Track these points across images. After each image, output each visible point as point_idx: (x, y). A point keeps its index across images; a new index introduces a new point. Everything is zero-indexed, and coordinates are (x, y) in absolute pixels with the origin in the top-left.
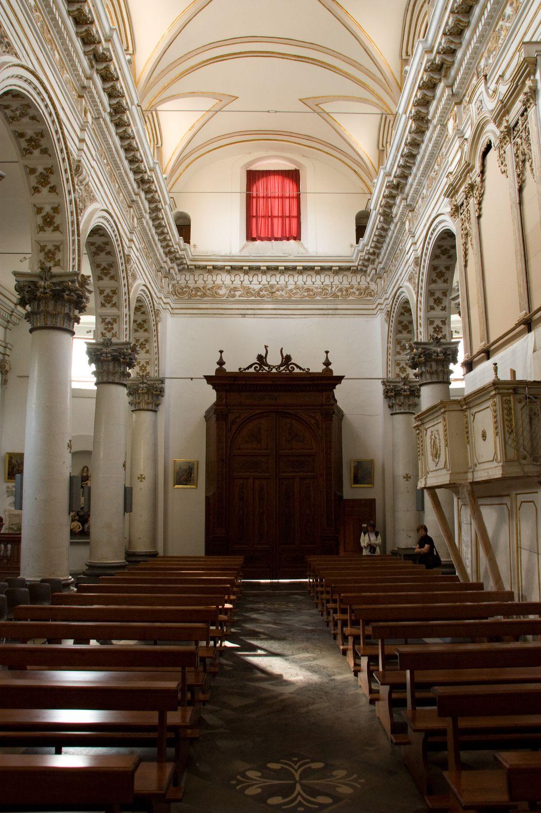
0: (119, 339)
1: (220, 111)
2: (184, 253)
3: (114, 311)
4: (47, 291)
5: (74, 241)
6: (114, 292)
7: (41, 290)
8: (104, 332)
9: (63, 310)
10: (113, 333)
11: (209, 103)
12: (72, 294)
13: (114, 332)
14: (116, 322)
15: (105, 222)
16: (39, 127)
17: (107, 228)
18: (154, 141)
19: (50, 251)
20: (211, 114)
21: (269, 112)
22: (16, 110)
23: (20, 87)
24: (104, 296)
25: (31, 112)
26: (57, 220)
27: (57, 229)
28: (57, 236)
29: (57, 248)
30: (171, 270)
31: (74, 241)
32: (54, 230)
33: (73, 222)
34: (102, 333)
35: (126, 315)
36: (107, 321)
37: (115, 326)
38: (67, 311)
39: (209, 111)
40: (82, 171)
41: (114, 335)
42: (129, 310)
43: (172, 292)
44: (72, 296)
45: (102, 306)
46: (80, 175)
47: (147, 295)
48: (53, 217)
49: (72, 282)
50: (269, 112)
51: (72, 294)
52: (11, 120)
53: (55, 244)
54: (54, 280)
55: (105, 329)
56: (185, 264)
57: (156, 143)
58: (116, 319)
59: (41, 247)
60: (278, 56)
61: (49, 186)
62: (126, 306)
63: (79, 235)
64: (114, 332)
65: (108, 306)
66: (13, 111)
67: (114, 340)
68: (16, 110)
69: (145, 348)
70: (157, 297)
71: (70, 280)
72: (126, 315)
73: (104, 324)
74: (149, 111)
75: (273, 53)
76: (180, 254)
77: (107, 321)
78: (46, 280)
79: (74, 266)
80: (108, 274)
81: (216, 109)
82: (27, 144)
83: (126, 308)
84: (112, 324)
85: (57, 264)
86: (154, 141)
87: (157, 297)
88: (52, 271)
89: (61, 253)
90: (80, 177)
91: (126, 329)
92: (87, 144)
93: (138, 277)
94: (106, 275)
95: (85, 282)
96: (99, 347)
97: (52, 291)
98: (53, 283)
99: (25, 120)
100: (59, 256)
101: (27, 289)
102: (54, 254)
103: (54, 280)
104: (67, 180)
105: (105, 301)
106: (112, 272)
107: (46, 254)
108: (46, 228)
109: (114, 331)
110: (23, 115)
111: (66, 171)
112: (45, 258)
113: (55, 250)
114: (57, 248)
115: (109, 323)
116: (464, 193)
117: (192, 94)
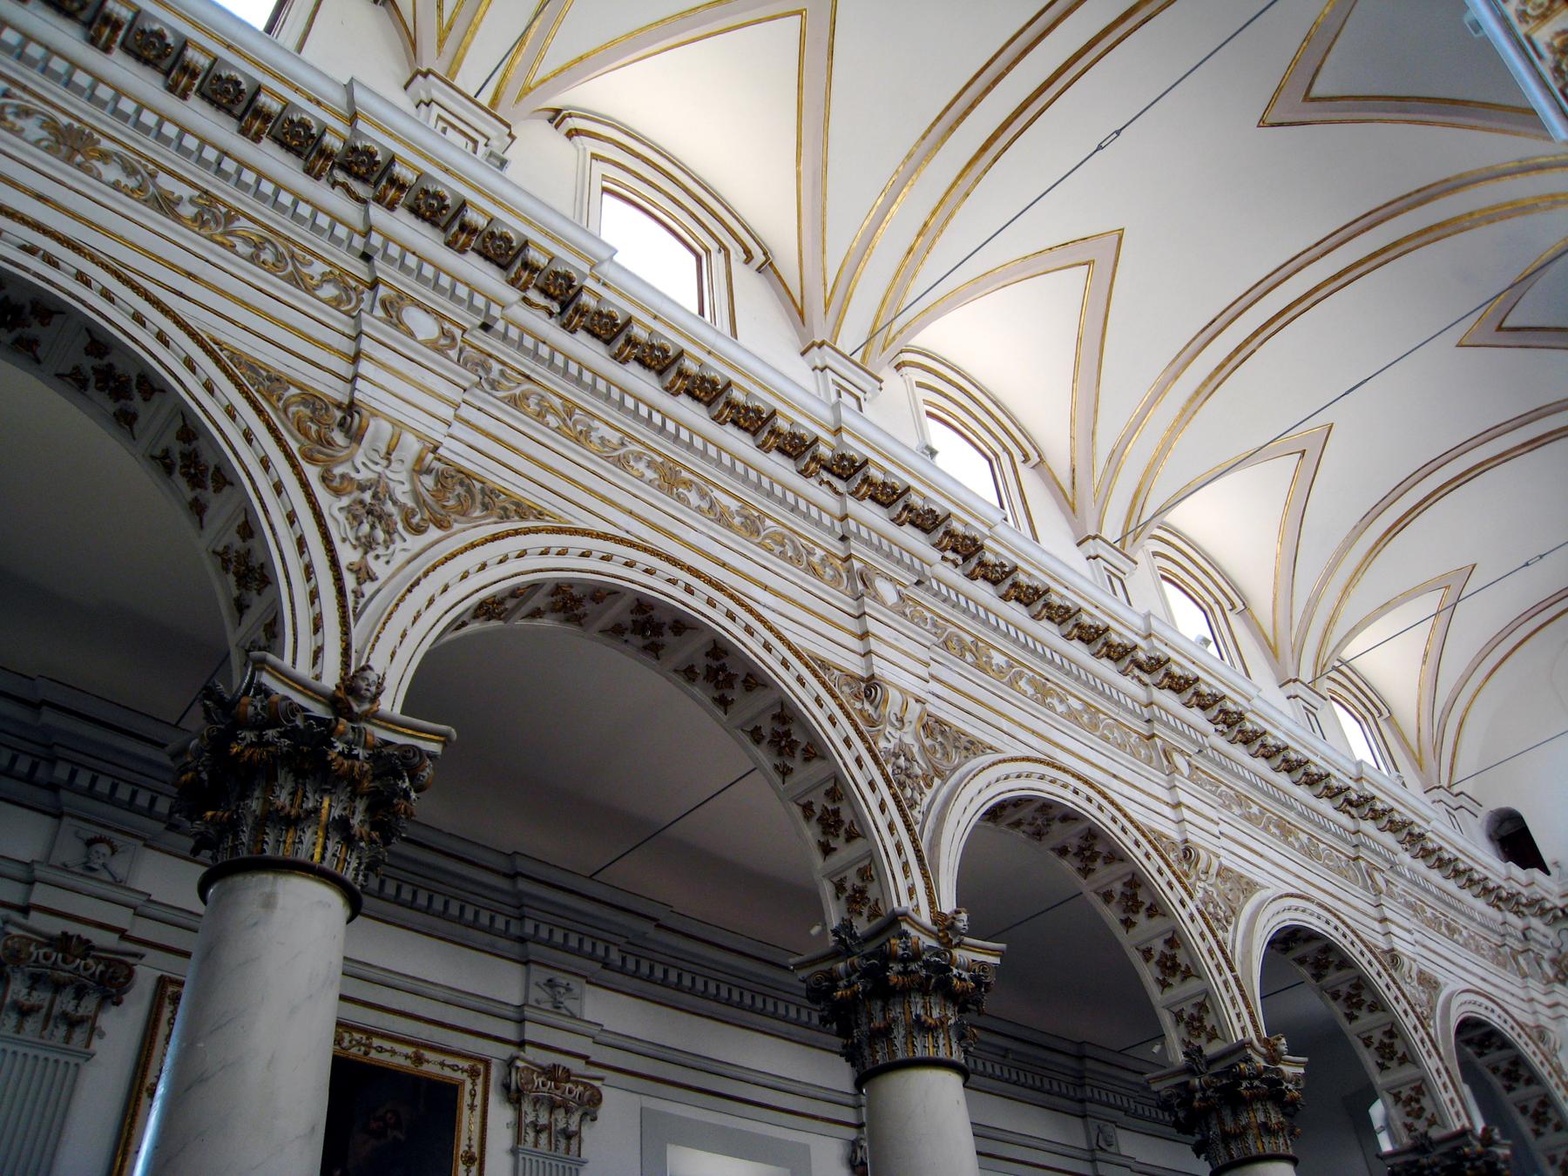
0: (1445, 1127)
1: (1458, 601)
2: (1531, 889)
3: (1408, 1072)
4: (1209, 1093)
5: (1226, 982)
6: (1391, 1034)
7: (1198, 1095)
8: (1409, 1120)
9: (1253, 1120)
10: (1427, 1119)
11: (1429, 603)
12: (1256, 1083)
13: (1429, 1116)
14: (1423, 1094)
15: (1298, 915)
16: (1081, 827)
17: (1310, 923)
18: (1372, 714)
19: (1192, 1016)
20: (1445, 615)
21: (1527, 564)
22: (1035, 819)
23: (1029, 789)
24: (1376, 1049)
25: (1056, 812)
26: (1182, 958)
27: (1187, 974)
28: (1193, 985)
29: (1201, 1006)
30: (1526, 932)
31: (1226, 982)
32: (1184, 979)
33: (1211, 951)
34: (1406, 1125)
35: (1438, 1071)
36: (1403, 1096)
37: (1426, 1102)
38: (1261, 1118)
39: (1438, 612)
40: (1198, 855)
41: (1432, 1122)
42: (1441, 1059)
43: (1556, 976)
44: (1257, 1087)
45: (1382, 1069)
46: (1196, 864)
47: (1486, 1008)
48: (1174, 957)
49: (1246, 1062)
50: (1527, 564)
51: (1256, 1083)
52: (1038, 835)
53: (1195, 1001)
54: (1217, 1068)
55: (1408, 1114)
56: (1551, 909)
57: (1376, 715)
58: (1420, 1087)
59: (1176, 1015)
60: (1495, 462)
61: (1145, 907)
62: (1428, 1052)
63: (1232, 970)
64: (1429, 1116)
65: (1393, 1064)
66: (1030, 824)
67: (1435, 1133)
68: (1035, 819)
69: (1550, 1120)
70: (1523, 1000)
71: (1241, 1057)
72: (1438, 1071)
73: (1400, 1105)
74: (1321, 676)
75: (1482, 464)
76: (1526, 894)
77: (1403, 1096)
78: (1202, 1073)
79: (1243, 1029)
80: (1362, 1005)
81: (1449, 601)
82: (1079, 859)
83: (1430, 1056)
84: (1418, 1101)
85: (1212, 1036)
86: (1372, 714)
87: (1523, 1000)
88: (1204, 1053)
89: (1212, 1014)
90: (1199, 866)
91: (1452, 1101)
92: (1188, 808)
93: (1441, 979)
94: (1359, 1005)
95: (1275, 1050)
96: (1411, 1157)
97: (1217, 1090)
98: (1216, 1075)
99: (1056, 826)
100: (1209, 1021)
101: (1176, 1102)
102: (1201, 1020)
103: (1217, 1068)
104: (1170, 884)
105: (1382, 1057)
106: (1367, 997)
107: (1187, 1024)
108: (1170, 980)
109: (1427, 1114)
110: (1048, 824)
111: (1160, 872)
112: (1189, 1033)
113: (1199, 1012)
114: (1201, 1006)
115: (1411, 1099)
116: (1353, 771)
117: (1386, 607)
